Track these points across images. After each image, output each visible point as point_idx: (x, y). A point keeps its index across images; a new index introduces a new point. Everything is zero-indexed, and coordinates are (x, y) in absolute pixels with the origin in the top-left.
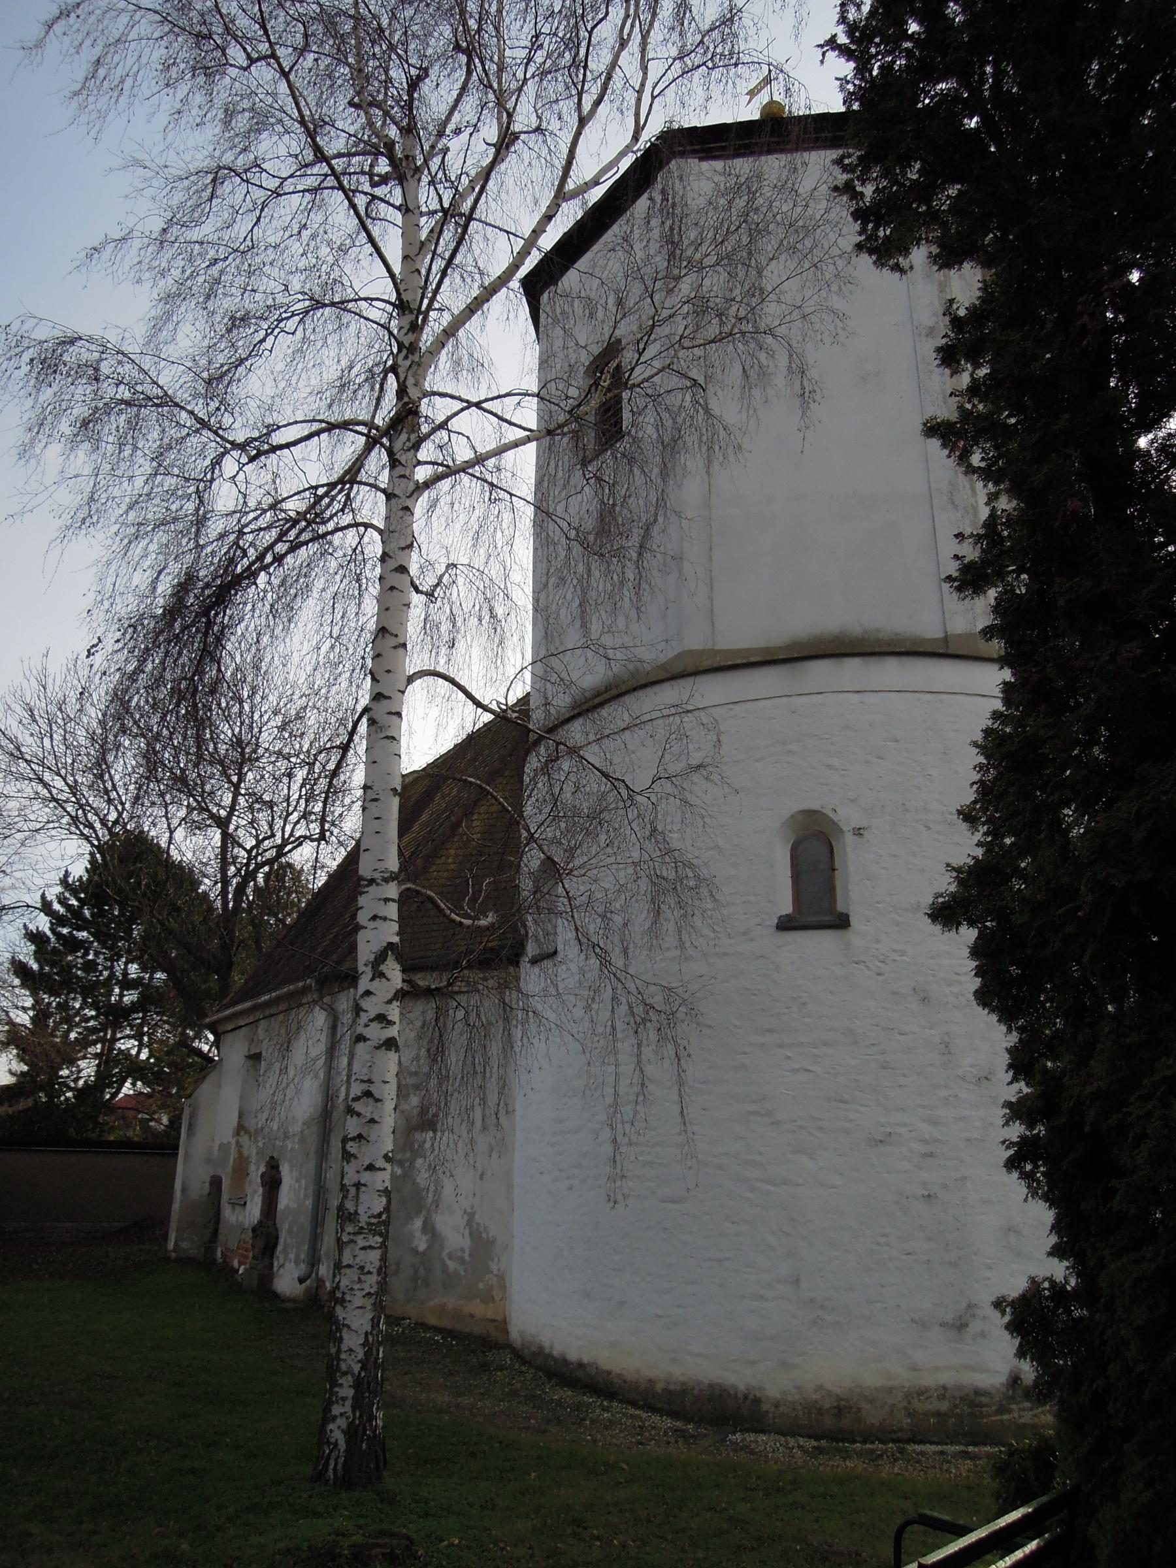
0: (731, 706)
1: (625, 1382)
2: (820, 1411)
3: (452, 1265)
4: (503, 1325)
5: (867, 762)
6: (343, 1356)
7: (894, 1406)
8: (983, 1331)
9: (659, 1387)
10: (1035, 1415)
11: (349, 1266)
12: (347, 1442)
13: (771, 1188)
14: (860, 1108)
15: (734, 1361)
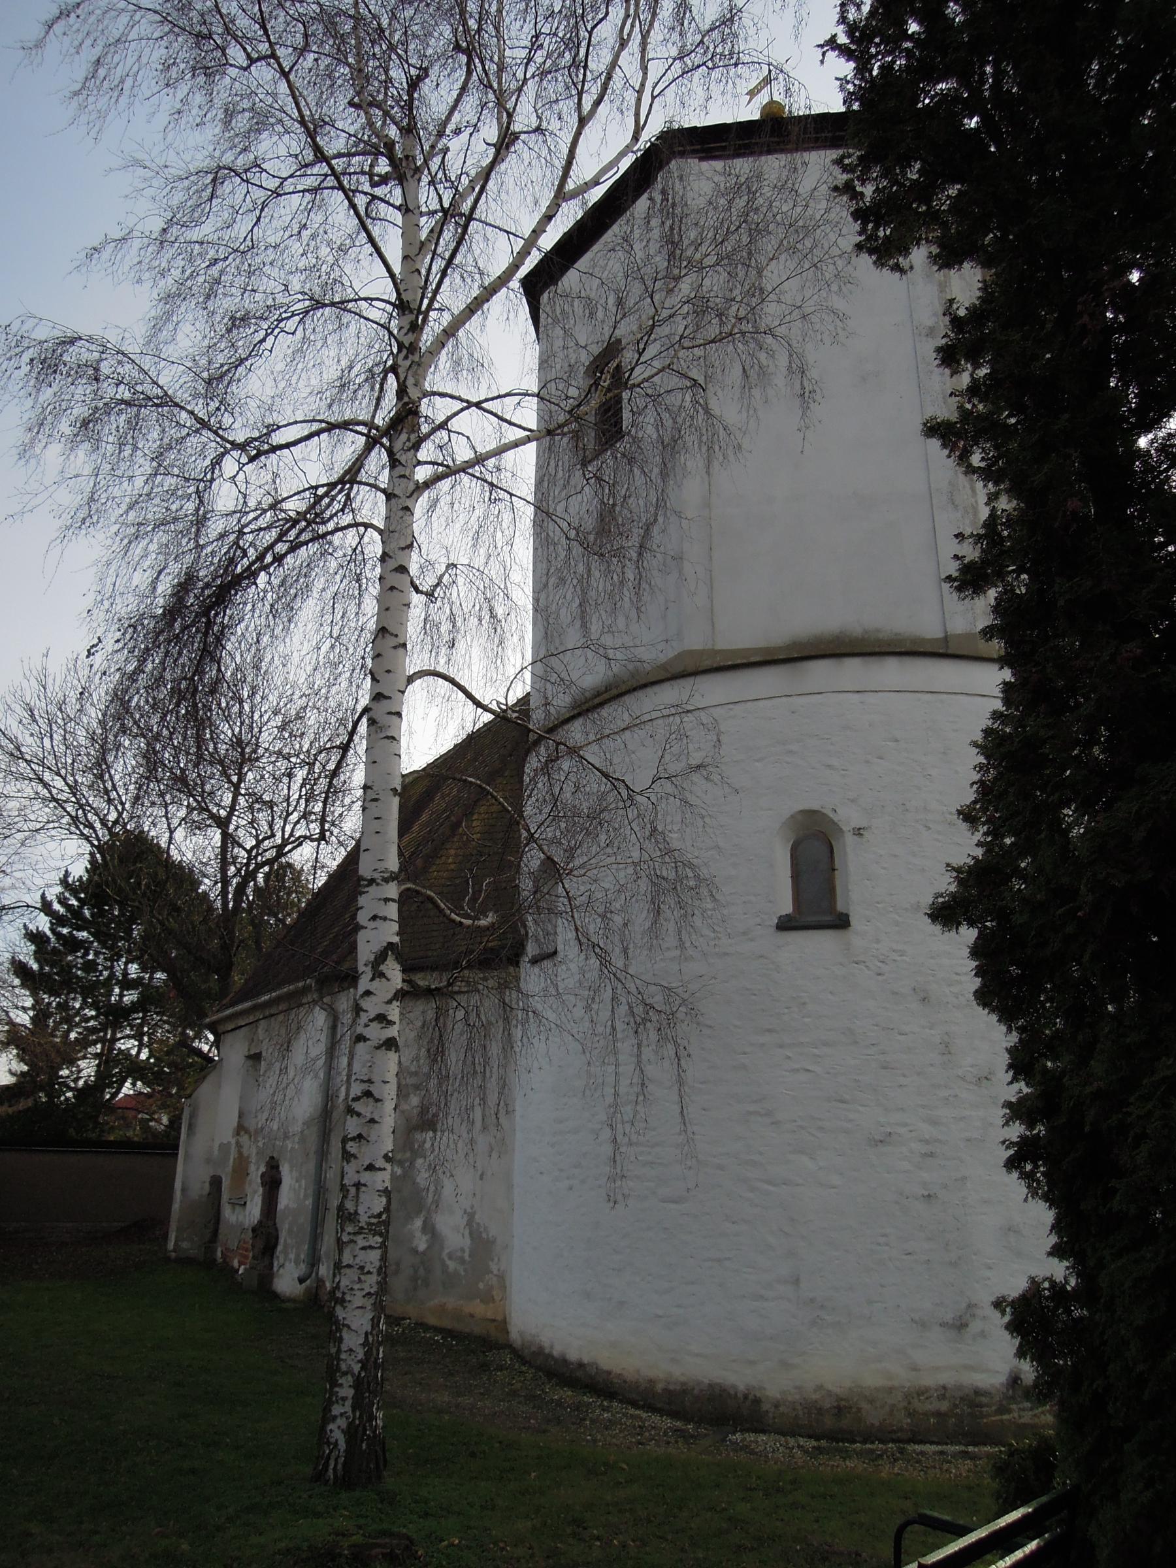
0: (731, 706)
1: (625, 1382)
2: (820, 1411)
3: (452, 1265)
4: (503, 1325)
5: (867, 762)
6: (343, 1356)
7: (894, 1406)
8: (983, 1331)
9: (659, 1387)
10: (1035, 1415)
11: (349, 1266)
12: (347, 1442)
13: (771, 1188)
14: (860, 1108)
15: (734, 1361)
